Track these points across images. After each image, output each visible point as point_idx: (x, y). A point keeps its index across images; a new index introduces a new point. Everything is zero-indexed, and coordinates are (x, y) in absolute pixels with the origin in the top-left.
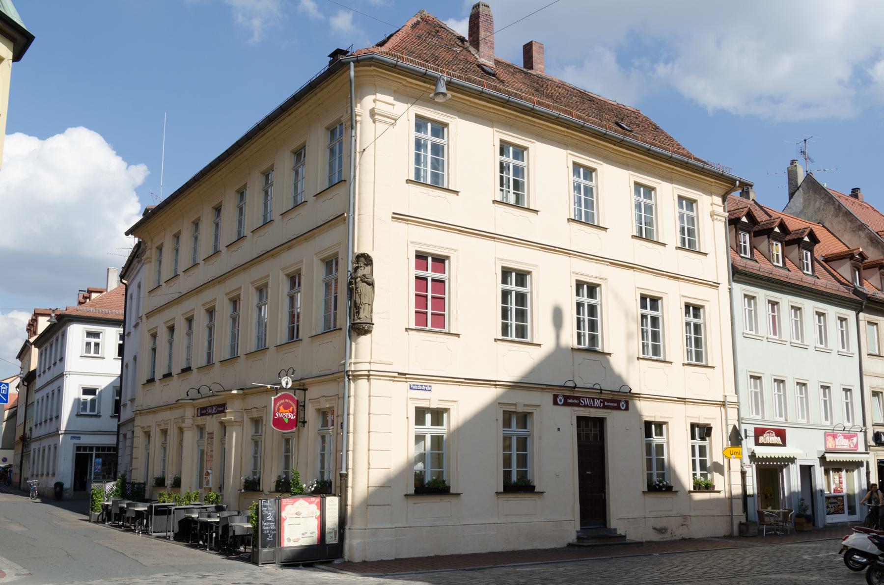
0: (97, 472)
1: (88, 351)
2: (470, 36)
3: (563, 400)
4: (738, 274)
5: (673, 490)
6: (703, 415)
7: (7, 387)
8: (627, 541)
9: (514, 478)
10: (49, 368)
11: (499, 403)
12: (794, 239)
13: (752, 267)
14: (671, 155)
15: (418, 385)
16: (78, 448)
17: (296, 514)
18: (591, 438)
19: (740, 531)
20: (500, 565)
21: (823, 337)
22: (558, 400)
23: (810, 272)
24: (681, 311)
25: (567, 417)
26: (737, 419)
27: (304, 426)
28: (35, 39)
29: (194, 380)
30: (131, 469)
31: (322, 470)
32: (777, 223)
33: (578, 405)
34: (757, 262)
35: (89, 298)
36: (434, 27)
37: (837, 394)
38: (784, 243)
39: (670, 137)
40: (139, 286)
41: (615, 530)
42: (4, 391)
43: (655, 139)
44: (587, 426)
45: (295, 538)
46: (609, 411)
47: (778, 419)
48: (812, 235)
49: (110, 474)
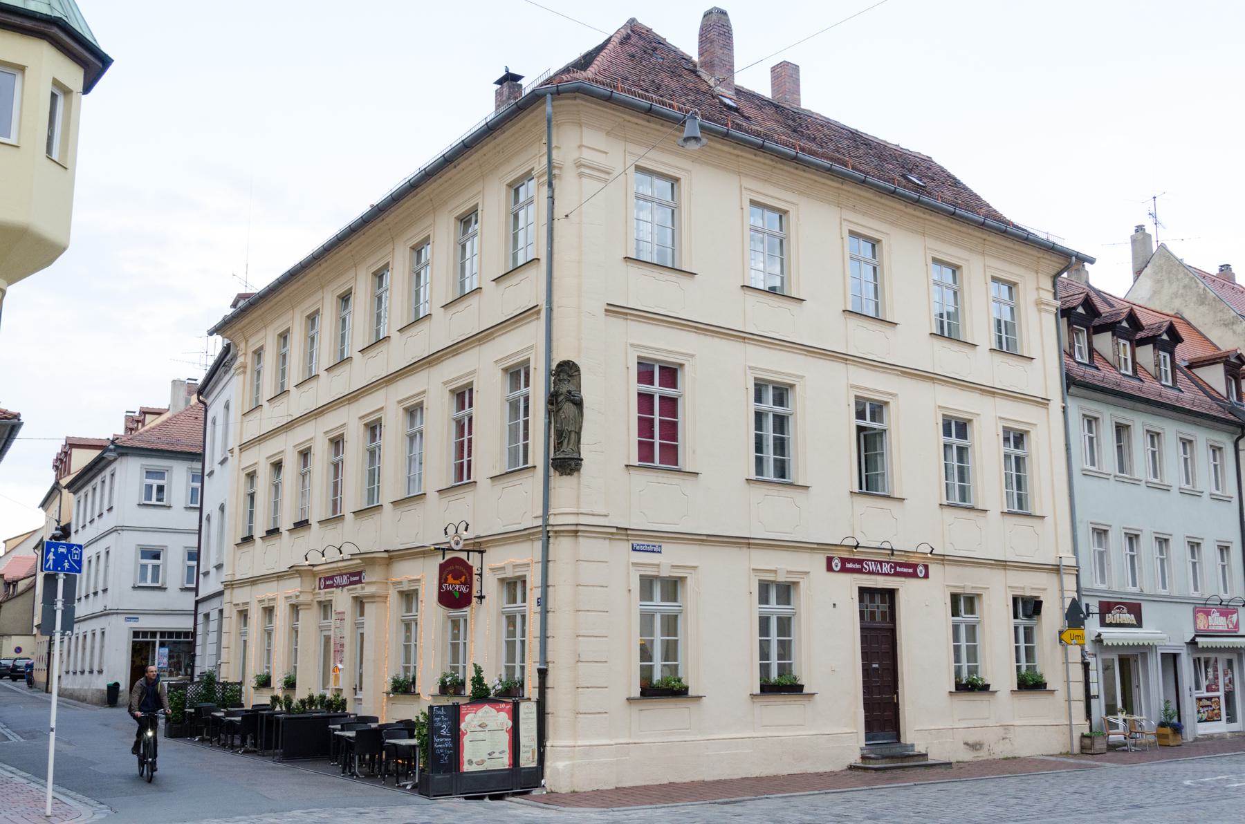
0: (162, 668)
1: (149, 497)
2: (701, 54)
3: (840, 564)
4: (1071, 383)
5: (1048, 688)
6: (1029, 584)
7: (80, 550)
8: (930, 762)
9: (774, 675)
10: (92, 521)
11: (753, 569)
12: (1148, 338)
13: (1090, 374)
14: (953, 210)
15: (643, 545)
16: (136, 634)
17: (480, 726)
18: (878, 618)
19: (1082, 748)
20: (763, 796)
21: (1123, 461)
22: (833, 564)
23: (1170, 384)
24: (938, 428)
25: (846, 588)
26: (1076, 589)
27: (481, 603)
28: (113, 64)
29: (315, 538)
30: (219, 663)
31: (522, 664)
32: (1125, 314)
33: (859, 571)
34: (1099, 370)
35: (143, 422)
36: (650, 43)
37: (1209, 553)
38: (1134, 342)
39: (976, 195)
40: (227, 407)
41: (913, 745)
42: (76, 556)
43: (956, 198)
44: (872, 601)
45: (479, 759)
46: (903, 579)
47: (1130, 589)
48: (1171, 330)
49: (181, 670)
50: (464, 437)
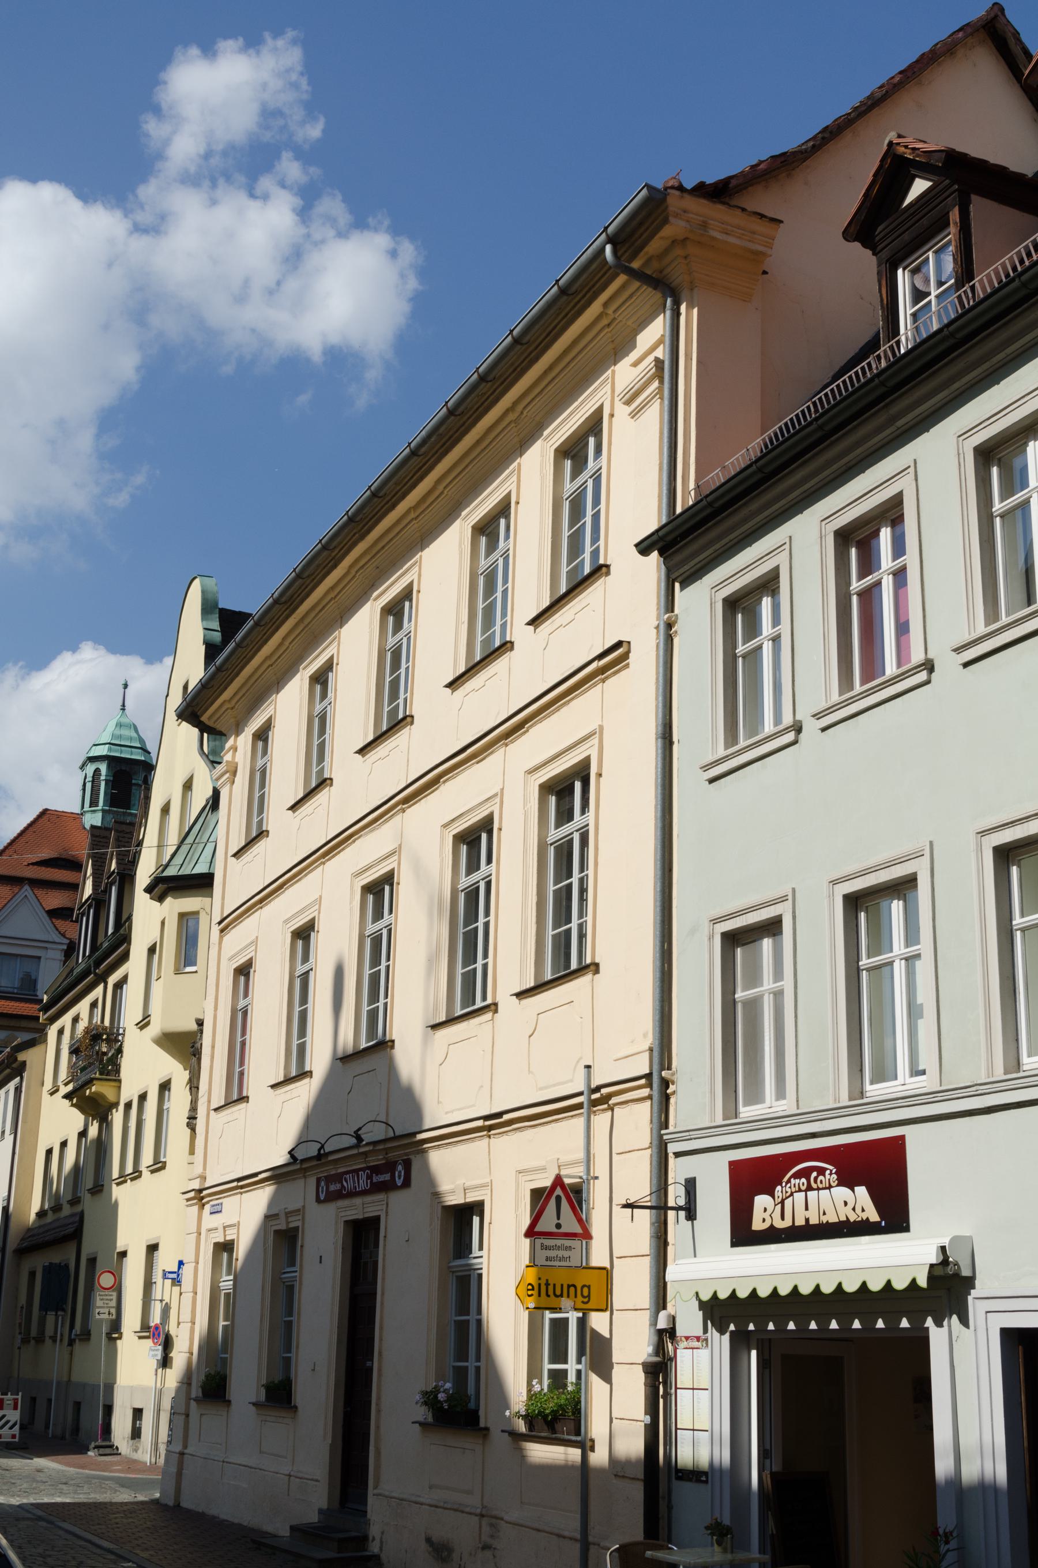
50: (570, 922)
